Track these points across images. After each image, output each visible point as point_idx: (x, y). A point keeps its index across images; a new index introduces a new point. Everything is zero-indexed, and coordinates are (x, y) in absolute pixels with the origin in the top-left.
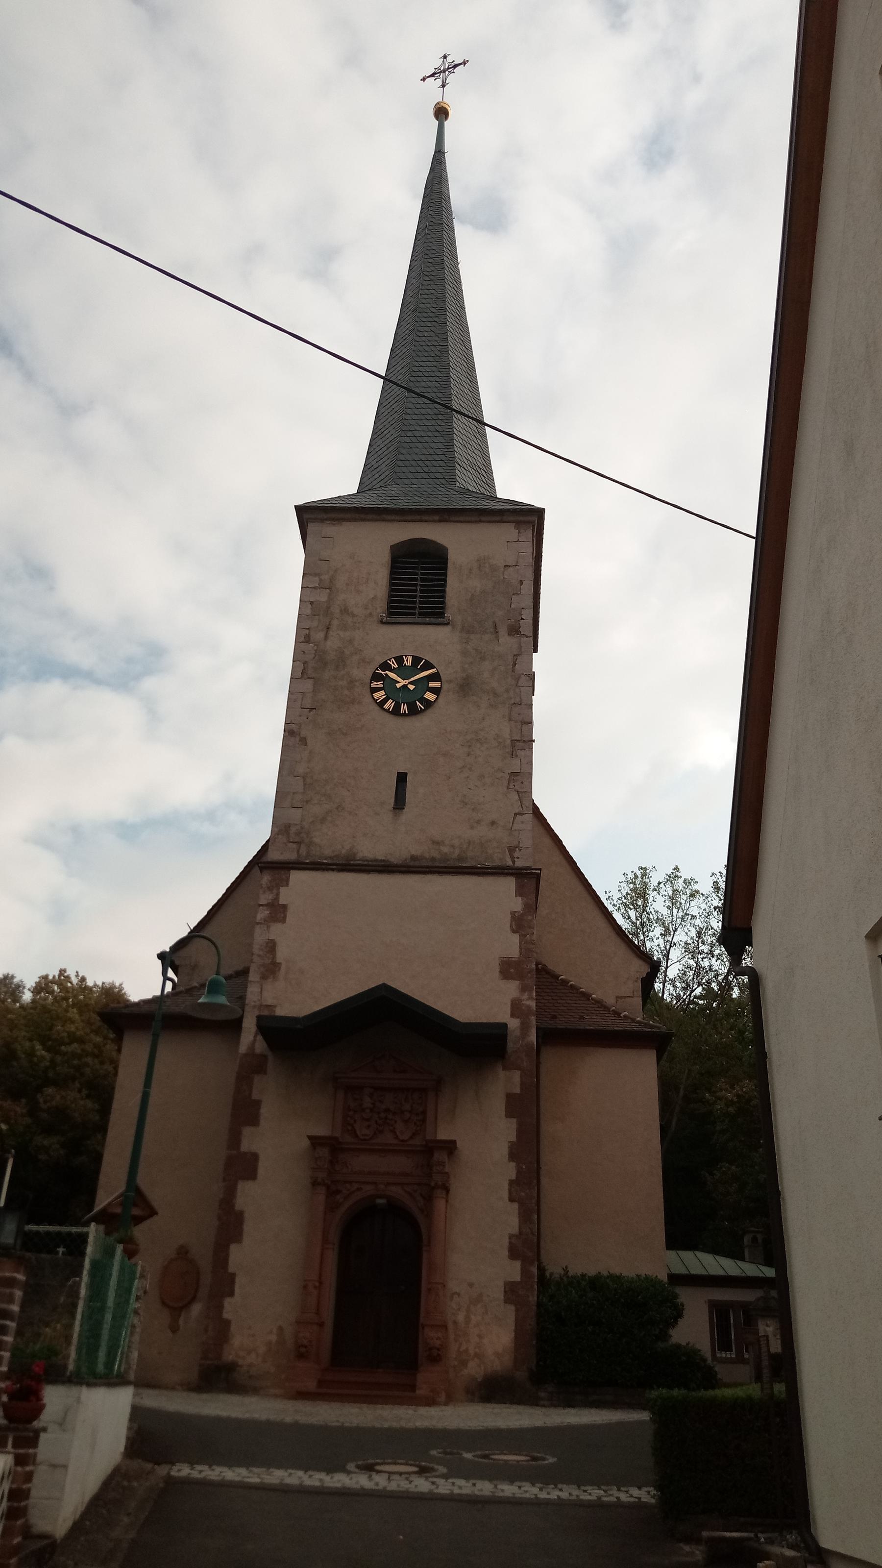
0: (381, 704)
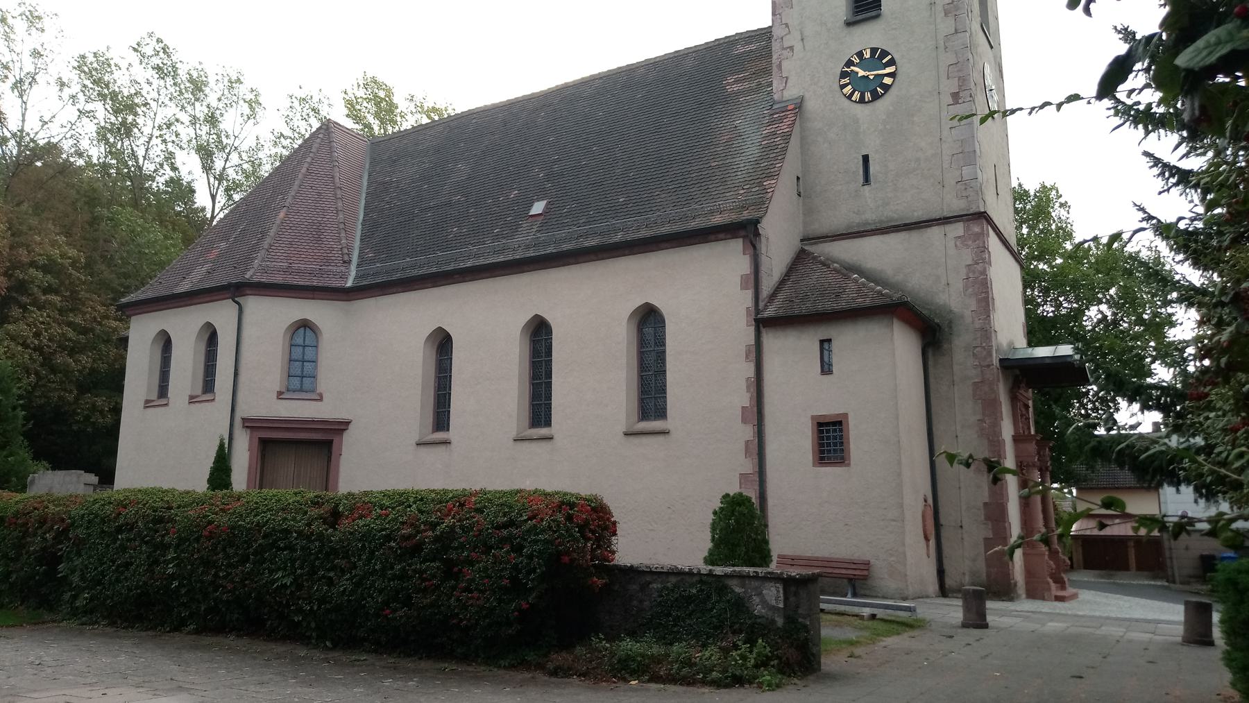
0: (850, 97)
